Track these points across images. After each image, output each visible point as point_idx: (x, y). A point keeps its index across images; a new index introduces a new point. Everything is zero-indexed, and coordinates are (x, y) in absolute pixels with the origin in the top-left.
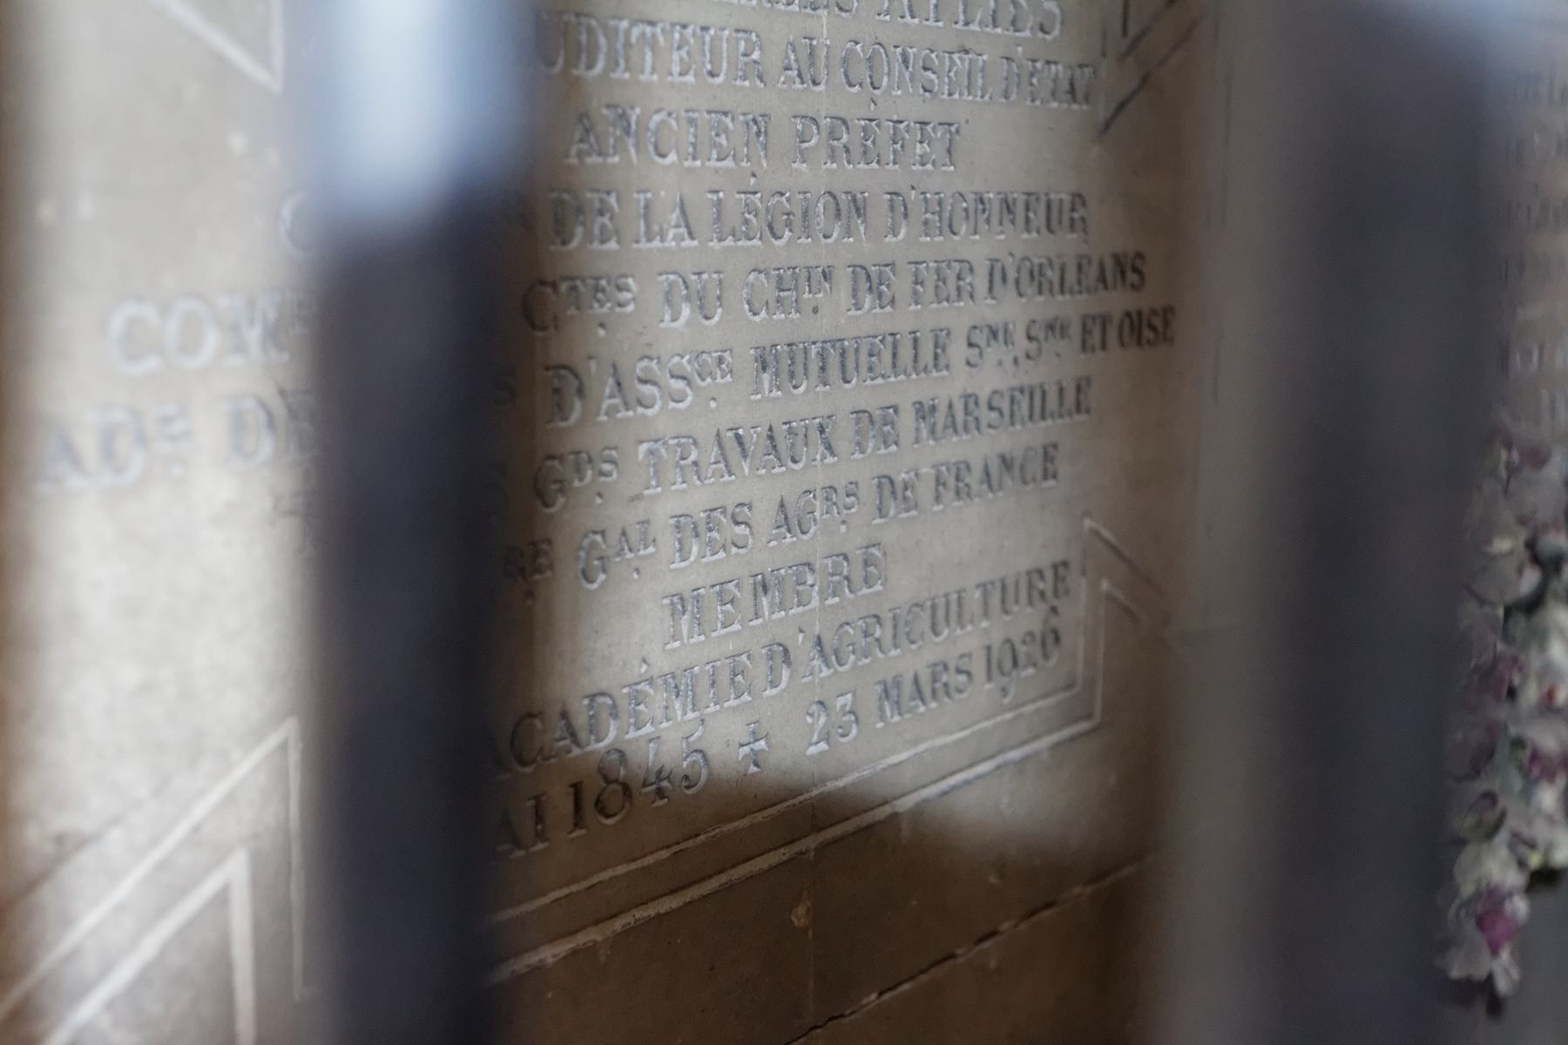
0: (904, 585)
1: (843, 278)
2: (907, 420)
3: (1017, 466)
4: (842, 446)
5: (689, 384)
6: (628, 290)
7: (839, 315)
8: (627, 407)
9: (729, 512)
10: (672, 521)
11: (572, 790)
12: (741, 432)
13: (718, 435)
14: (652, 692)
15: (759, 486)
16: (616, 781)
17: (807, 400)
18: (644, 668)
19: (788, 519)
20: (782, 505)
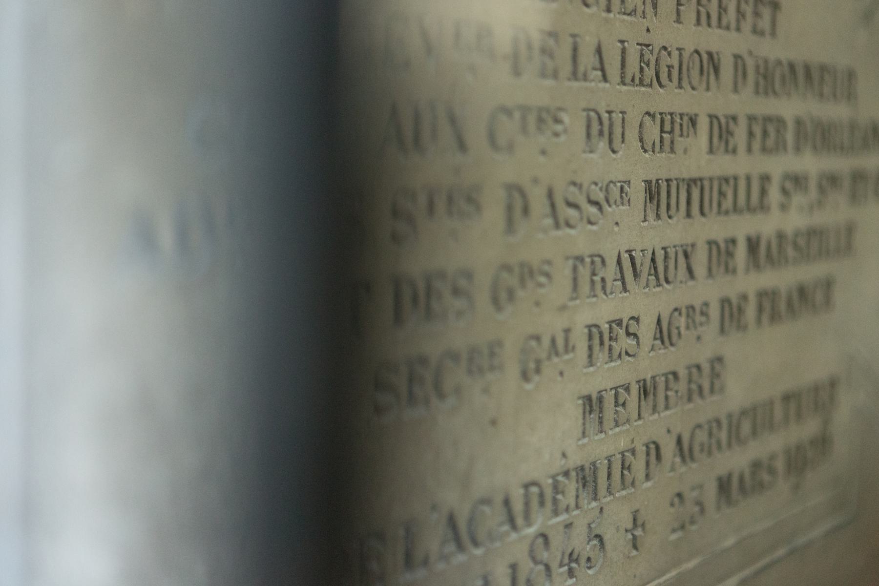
0: (736, 393)
1: (703, 124)
2: (741, 252)
3: (585, 220)
4: (700, 270)
5: (600, 209)
6: (629, 394)
7: (695, 158)
8: (557, 226)
9: (624, 324)
10: (585, 114)
11: (509, 571)
12: (634, 253)
13: (619, 256)
14: (566, 481)
15: (646, 303)
16: (541, 562)
17: (672, 232)
18: (563, 462)
19: (664, 335)
20: (659, 321)
